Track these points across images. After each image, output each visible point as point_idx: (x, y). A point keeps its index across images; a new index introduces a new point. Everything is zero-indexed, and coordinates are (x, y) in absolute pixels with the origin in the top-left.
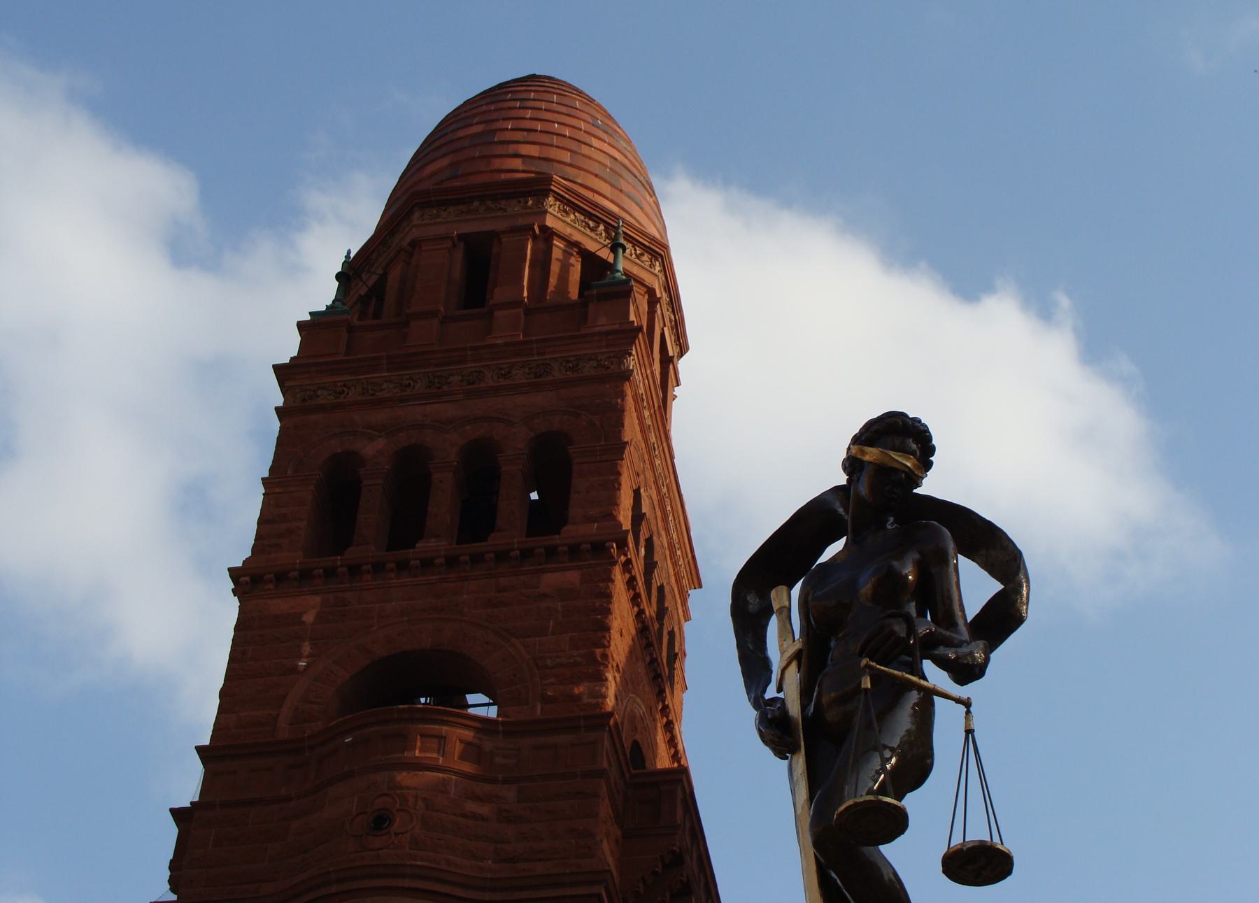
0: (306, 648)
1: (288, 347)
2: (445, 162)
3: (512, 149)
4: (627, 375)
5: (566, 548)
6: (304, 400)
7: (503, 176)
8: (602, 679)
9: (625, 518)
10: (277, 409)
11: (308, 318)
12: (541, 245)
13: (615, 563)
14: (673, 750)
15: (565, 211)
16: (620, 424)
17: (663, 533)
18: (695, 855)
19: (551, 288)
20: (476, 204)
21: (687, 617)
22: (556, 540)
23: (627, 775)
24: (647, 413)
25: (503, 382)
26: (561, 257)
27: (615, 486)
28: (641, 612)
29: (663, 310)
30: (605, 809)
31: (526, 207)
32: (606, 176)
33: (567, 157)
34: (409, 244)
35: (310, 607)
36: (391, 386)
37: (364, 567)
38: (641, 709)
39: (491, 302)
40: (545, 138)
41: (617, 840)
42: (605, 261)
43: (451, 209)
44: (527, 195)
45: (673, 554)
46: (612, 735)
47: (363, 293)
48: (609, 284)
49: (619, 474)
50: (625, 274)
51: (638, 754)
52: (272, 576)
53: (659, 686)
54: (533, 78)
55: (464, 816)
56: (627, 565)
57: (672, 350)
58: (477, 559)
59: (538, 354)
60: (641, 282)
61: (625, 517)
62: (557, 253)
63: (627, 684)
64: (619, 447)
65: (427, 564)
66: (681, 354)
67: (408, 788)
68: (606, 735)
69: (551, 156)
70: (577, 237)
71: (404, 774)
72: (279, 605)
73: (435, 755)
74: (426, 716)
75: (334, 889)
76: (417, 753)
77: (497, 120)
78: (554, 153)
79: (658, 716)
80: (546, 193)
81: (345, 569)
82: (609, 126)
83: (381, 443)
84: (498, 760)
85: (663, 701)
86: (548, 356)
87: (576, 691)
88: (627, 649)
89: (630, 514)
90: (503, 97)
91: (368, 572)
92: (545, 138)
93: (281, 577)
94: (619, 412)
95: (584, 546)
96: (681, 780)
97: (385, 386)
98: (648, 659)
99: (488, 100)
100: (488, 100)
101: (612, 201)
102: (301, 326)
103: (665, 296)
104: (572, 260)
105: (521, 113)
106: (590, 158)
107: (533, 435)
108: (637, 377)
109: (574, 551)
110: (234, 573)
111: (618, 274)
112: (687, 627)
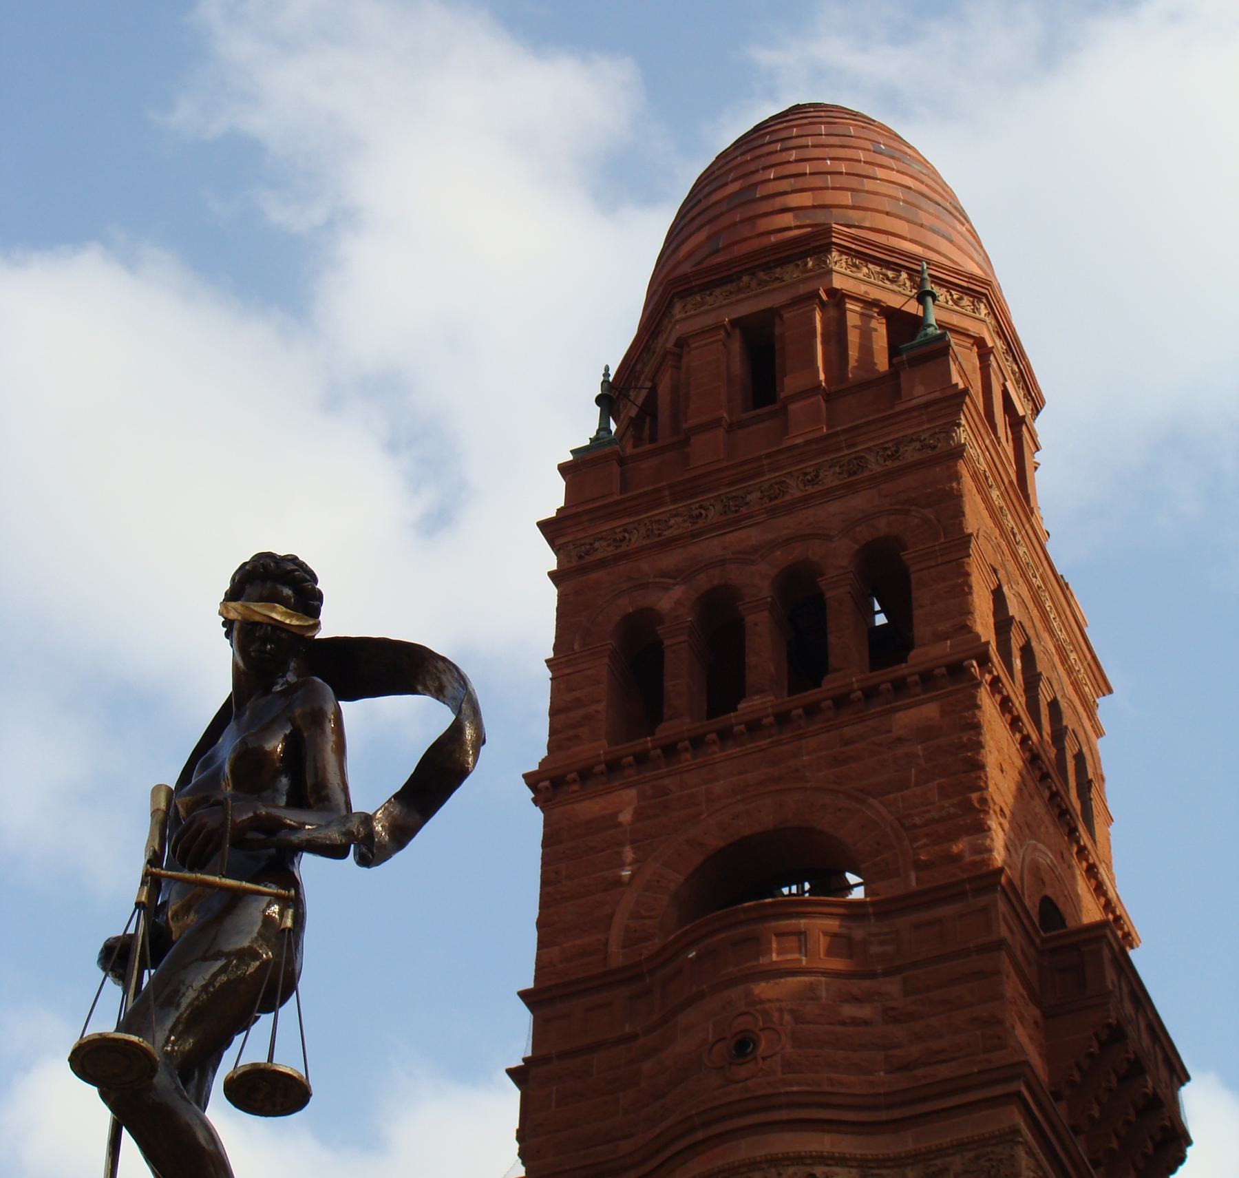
0: (629, 854)
2: (702, 236)
3: (779, 202)
4: (958, 452)
5: (916, 678)
6: (581, 557)
7: (773, 239)
8: (983, 829)
9: (985, 626)
10: (551, 574)
11: (571, 458)
12: (832, 313)
13: (979, 685)
14: (1102, 900)
15: (854, 265)
16: (960, 513)
17: (1046, 635)
18: (1142, 1025)
20: (745, 279)
21: (1099, 733)
22: (902, 670)
23: (1038, 941)
24: (995, 494)
25: (811, 489)
26: (859, 323)
27: (963, 590)
28: (1025, 739)
29: (1000, 362)
30: (1012, 986)
33: (847, 198)
34: (675, 345)
35: (624, 804)
36: (680, 519)
37: (680, 745)
38: (1046, 857)
39: (782, 395)
40: (817, 182)
41: (1036, 1023)
42: (916, 316)
43: (718, 291)
44: (804, 256)
45: (1064, 660)
46: (1006, 895)
48: (921, 344)
49: (968, 575)
50: (941, 327)
51: (1052, 912)
52: (574, 775)
53: (1068, 824)
54: (798, 107)
55: (843, 1023)
56: (995, 683)
57: (1021, 408)
58: (811, 710)
59: (848, 447)
60: (964, 333)
61: (984, 626)
62: (853, 320)
63: (1022, 828)
64: (964, 541)
65: (754, 727)
66: (1036, 411)
67: (769, 1001)
68: (999, 896)
70: (875, 294)
71: (763, 984)
72: (589, 808)
73: (796, 956)
74: (795, 907)
75: (700, 1135)
76: (775, 957)
77: (757, 171)
78: (830, 197)
79: (1075, 861)
80: (827, 248)
81: (659, 751)
83: (678, 591)
84: (875, 949)
85: (1078, 842)
86: (860, 448)
87: (955, 849)
88: (1013, 788)
89: (991, 620)
90: (760, 142)
91: (686, 749)
92: (817, 182)
93: (585, 775)
94: (953, 505)
95: (937, 671)
96: (1105, 936)
98: (1047, 794)
99: (744, 148)
100: (744, 148)
101: (911, 241)
102: (564, 469)
103: (999, 343)
104: (874, 324)
105: (784, 156)
106: (876, 193)
107: (856, 547)
108: (973, 451)
109: (927, 679)
110: (532, 780)
111: (930, 330)
112: (1101, 745)
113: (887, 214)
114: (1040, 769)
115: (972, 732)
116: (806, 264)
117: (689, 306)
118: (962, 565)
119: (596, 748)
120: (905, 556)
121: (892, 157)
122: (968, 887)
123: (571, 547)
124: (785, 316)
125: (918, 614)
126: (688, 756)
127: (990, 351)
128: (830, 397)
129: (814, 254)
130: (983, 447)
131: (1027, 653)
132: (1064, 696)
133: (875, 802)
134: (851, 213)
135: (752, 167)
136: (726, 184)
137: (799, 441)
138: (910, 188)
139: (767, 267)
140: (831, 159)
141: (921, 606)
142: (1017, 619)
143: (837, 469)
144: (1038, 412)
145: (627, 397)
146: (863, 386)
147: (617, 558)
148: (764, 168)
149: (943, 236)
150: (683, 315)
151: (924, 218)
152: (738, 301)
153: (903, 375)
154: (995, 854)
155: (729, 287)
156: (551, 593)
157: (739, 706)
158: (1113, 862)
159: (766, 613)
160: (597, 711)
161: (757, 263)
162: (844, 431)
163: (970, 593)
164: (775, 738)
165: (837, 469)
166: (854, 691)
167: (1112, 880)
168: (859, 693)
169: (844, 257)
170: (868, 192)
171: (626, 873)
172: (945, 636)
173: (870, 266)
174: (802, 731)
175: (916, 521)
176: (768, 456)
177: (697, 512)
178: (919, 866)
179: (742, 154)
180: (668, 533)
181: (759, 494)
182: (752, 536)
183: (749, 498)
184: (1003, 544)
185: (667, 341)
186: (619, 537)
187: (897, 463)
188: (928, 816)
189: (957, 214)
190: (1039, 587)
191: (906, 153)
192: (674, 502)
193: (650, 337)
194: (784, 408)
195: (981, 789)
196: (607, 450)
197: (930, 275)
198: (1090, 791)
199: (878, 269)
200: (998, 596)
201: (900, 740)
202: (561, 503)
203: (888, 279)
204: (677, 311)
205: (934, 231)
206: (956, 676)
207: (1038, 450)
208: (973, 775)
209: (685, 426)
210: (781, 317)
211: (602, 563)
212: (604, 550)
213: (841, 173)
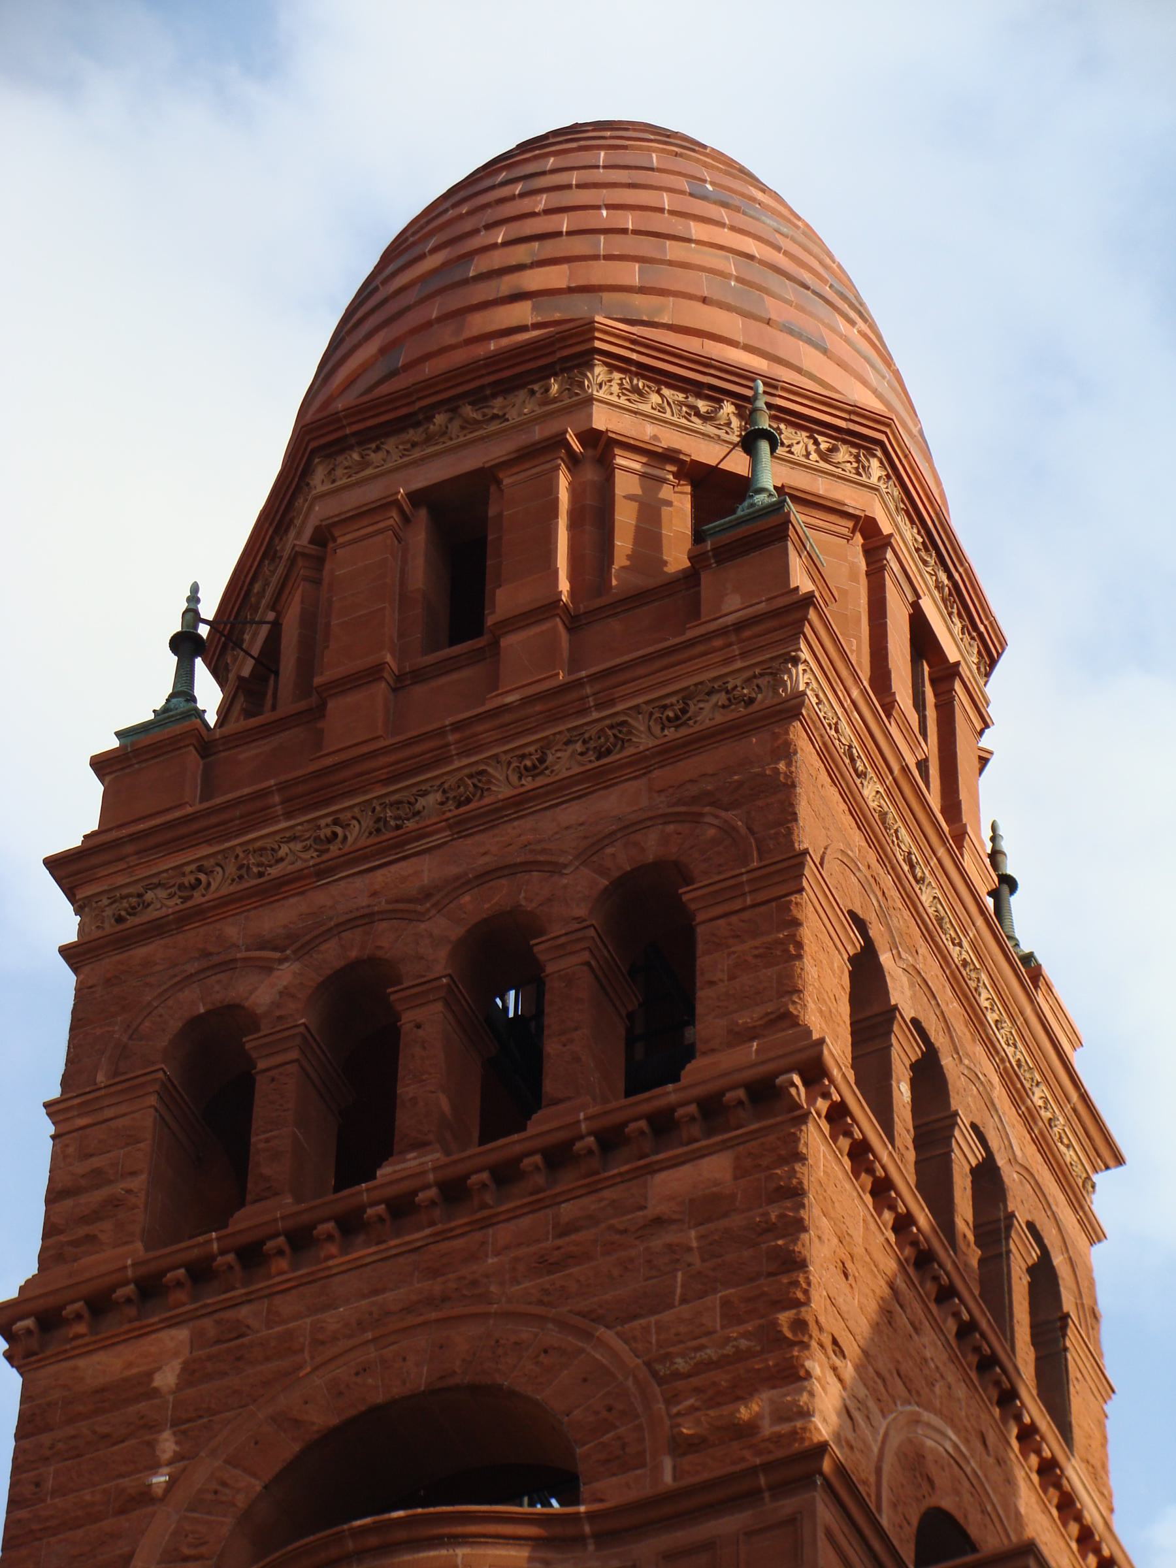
0: (167, 1444)
1: (76, 811)
2: (371, 348)
3: (507, 284)
5: (692, 1109)
6: (120, 920)
7: (492, 346)
8: (795, 1376)
9: (828, 1016)
12: (590, 474)
13: (804, 1118)
14: (1074, 1528)
15: (636, 390)
17: (979, 1050)
19: (620, 559)
20: (440, 419)
21: (1095, 1234)
22: (669, 1094)
24: (870, 790)
25: (528, 783)
27: (785, 951)
28: (903, 1223)
31: (546, 401)
32: (730, 300)
33: (632, 274)
35: (165, 1355)
38: (942, 1439)
39: (490, 621)
43: (390, 444)
44: (545, 373)
47: (246, 672)
49: (796, 923)
52: (79, 1305)
57: (952, 642)
58: (505, 1175)
59: (599, 706)
60: (836, 510)
63: (885, 1376)
64: (790, 866)
65: (402, 1208)
66: (989, 660)
69: (595, 281)
70: (670, 439)
72: (104, 1365)
77: (476, 232)
78: (600, 273)
80: (585, 359)
81: (230, 1257)
82: (729, 185)
83: (287, 973)
85: (1018, 1418)
86: (620, 707)
87: (744, 1413)
88: (872, 1306)
89: (844, 1009)
91: (280, 1253)
92: (579, 246)
93: (99, 1305)
94: (776, 799)
97: (284, 850)
98: (951, 1326)
101: (748, 348)
102: (101, 764)
104: (666, 492)
109: (712, 1110)
113: (704, 300)
114: (936, 1279)
115: (788, 1204)
116: (547, 390)
117: (339, 472)
118: (787, 908)
119: (120, 1255)
120: (687, 894)
121: (725, 205)
122: (762, 1481)
123: (105, 901)
124: (506, 481)
125: (704, 997)
126: (283, 1263)
127: (887, 542)
128: (575, 622)
129: (563, 371)
130: (847, 703)
131: (929, 1074)
132: (1013, 1160)
133: (608, 1335)
134: (638, 300)
135: (468, 225)
136: (422, 257)
137: (509, 699)
138: (751, 257)
139: (479, 398)
140: (608, 207)
141: (712, 983)
142: (909, 1013)
143: (579, 747)
144: (993, 663)
145: (238, 644)
146: (636, 599)
147: (183, 920)
148: (488, 227)
149: (810, 342)
150: (328, 486)
151: (772, 308)
152: (423, 459)
153: (705, 578)
154: (817, 1420)
155: (412, 435)
156: (64, 982)
157: (379, 1173)
158: (1112, 1466)
159: (439, 1006)
160: (129, 1191)
161: (460, 390)
162: (593, 678)
163: (800, 957)
164: (439, 1227)
165: (579, 747)
166: (581, 1137)
167: (1106, 1496)
168: (591, 1139)
169: (617, 376)
170: (671, 263)
171: (160, 1479)
172: (750, 1034)
173: (666, 391)
174: (485, 1213)
175: (712, 832)
176: (457, 727)
177: (328, 831)
178: (682, 1447)
179: (454, 206)
180: (274, 872)
181: (439, 796)
182: (423, 871)
183: (422, 802)
184: (887, 881)
185: (299, 538)
186: (189, 879)
187: (684, 731)
188: (700, 1356)
189: (845, 307)
190: (965, 963)
191: (754, 200)
192: (288, 815)
193: (276, 532)
194: (495, 644)
195: (797, 1304)
196: (178, 728)
197: (769, 406)
198: (1064, 1335)
199: (681, 397)
200: (866, 972)
201: (659, 1222)
202: (92, 823)
203: (698, 414)
204: (319, 481)
205: (791, 332)
206: (764, 1105)
207: (987, 726)
208: (785, 1280)
209: (318, 680)
210: (498, 482)
211: (157, 929)
212: (162, 903)
213: (624, 231)
